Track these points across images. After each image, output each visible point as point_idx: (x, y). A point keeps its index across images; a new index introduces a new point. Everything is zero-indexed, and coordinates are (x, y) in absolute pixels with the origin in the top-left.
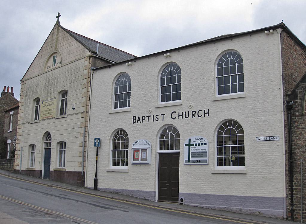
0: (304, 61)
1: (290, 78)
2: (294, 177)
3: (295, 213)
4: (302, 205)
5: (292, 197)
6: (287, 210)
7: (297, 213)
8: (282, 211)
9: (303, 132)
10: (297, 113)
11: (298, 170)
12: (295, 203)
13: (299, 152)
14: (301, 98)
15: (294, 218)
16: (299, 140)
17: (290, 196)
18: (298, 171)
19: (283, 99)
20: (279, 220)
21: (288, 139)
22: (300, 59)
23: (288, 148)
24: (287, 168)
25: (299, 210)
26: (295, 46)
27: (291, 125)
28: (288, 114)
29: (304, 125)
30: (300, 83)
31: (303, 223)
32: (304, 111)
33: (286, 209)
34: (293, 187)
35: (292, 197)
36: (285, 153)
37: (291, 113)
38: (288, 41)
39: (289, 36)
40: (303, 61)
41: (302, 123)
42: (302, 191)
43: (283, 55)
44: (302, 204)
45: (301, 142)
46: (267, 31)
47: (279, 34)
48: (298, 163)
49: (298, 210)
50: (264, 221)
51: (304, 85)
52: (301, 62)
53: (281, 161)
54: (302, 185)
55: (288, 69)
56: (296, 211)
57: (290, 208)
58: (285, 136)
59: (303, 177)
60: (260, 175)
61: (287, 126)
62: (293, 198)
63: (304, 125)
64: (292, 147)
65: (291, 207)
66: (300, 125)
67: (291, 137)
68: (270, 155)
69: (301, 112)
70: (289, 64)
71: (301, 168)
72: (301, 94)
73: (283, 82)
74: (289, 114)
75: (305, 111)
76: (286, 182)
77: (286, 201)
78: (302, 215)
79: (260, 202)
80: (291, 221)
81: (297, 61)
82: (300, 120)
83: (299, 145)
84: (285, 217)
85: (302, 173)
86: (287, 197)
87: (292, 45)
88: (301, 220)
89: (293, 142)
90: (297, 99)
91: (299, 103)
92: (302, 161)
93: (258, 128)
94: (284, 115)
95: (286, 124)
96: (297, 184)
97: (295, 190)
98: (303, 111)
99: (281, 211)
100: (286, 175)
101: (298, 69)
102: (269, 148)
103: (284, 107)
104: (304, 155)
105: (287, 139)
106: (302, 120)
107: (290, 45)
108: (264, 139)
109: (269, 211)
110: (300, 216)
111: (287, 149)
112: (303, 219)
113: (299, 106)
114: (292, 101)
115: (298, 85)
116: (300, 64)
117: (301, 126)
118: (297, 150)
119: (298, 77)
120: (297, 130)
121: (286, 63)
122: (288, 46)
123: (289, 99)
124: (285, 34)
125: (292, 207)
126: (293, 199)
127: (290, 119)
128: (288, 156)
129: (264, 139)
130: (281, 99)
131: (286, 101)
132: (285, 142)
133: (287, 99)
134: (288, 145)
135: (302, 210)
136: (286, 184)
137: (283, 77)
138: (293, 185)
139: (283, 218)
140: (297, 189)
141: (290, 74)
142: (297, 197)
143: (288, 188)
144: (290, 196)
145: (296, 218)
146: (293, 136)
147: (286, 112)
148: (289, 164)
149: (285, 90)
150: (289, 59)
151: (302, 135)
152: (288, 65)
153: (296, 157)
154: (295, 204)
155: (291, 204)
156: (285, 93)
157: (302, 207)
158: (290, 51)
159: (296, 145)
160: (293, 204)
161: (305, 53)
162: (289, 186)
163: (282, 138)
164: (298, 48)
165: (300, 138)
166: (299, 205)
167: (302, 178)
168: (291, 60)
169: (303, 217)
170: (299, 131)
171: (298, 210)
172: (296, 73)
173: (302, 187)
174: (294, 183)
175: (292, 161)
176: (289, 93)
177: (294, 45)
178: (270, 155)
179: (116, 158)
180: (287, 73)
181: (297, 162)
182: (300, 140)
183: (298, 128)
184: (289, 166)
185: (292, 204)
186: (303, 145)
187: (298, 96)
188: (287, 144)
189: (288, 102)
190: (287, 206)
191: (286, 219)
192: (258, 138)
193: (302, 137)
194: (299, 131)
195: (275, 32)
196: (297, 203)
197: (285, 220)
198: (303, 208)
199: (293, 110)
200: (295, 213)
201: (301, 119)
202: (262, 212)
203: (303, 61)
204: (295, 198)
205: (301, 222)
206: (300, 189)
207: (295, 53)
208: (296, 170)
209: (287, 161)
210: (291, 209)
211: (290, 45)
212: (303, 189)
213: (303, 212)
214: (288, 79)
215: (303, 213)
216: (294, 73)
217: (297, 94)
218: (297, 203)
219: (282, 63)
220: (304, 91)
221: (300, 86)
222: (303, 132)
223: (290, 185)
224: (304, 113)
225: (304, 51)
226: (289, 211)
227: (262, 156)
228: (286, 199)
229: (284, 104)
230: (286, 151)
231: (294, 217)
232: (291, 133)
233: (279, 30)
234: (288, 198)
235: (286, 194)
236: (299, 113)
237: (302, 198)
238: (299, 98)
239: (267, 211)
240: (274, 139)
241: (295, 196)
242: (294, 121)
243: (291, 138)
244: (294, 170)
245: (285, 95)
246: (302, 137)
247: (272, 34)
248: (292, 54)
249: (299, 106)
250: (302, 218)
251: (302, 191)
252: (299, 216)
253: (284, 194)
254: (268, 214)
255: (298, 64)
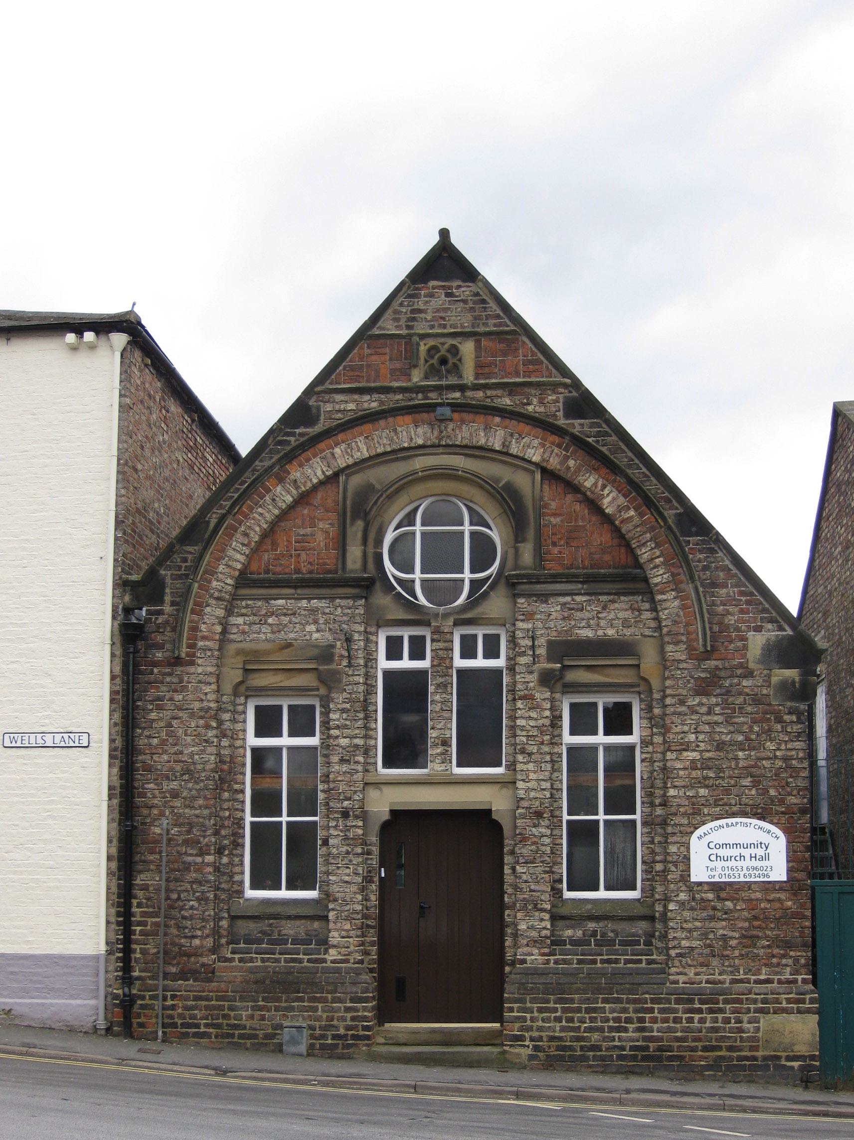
0: (189, 455)
1: (141, 522)
2: (138, 882)
3: (134, 1010)
4: (161, 978)
5: (127, 951)
6: (109, 999)
7: (142, 1007)
8: (93, 1002)
9: (175, 723)
10: (159, 655)
11: (151, 857)
12: (136, 974)
13: (157, 792)
14: (178, 599)
15: (135, 1025)
16: (160, 751)
17: (120, 950)
18: (152, 862)
19: (113, 597)
20: (81, 1035)
21: (120, 746)
22: (179, 449)
23: (121, 778)
24: (114, 851)
25: (152, 998)
26: (165, 402)
27: (133, 695)
28: (125, 654)
29: (181, 697)
30: (177, 547)
31: (163, 1041)
32: (184, 646)
33: (106, 997)
34: (133, 919)
35: (127, 951)
36: (109, 795)
37: (136, 652)
38: (143, 383)
39: (149, 362)
40: (185, 457)
41: (175, 691)
42: (161, 933)
43: (126, 432)
44: (161, 975)
45: (165, 757)
46: (73, 335)
47: (118, 355)
48: (154, 833)
49: (148, 997)
50: (26, 1041)
51: (190, 553)
52: (178, 461)
53: (92, 822)
54: (163, 910)
55: (136, 485)
56: (139, 1002)
57: (120, 992)
58: (110, 734)
59: (167, 880)
60: (15, 873)
61: (119, 697)
62: (133, 956)
63: (181, 697)
64: (132, 775)
65: (123, 988)
66: (168, 696)
67: (133, 737)
68: (51, 802)
69: (174, 653)
70: (139, 467)
71: (164, 849)
72: (178, 584)
73: (115, 535)
74: (131, 656)
75: (188, 647)
76: (108, 900)
77: (106, 967)
78: (160, 1015)
79: (12, 973)
80: (121, 1038)
81: (166, 456)
82: (168, 679)
83: (159, 767)
84: (102, 1024)
85: (164, 866)
86: (109, 953)
87: (154, 398)
88: (156, 1032)
89: (140, 758)
90: (161, 602)
91: (170, 615)
92: (168, 824)
93: (13, 698)
94: (113, 655)
95: (118, 688)
96: (147, 907)
97: (139, 928)
98: (179, 648)
99: (86, 1002)
100: (110, 873)
101: (168, 488)
102: (51, 775)
103: (112, 626)
104: (176, 804)
105: (119, 743)
106: (175, 680)
107: (150, 396)
108: (32, 740)
109: (43, 1005)
110: (154, 1020)
111: (117, 783)
112: (163, 1027)
113: (168, 629)
114: (144, 609)
115: (169, 551)
116: (175, 466)
117: (171, 699)
118: (151, 786)
119: (165, 518)
120: (153, 715)
121: (130, 464)
122: (142, 402)
123: (132, 600)
124: (138, 354)
125: (126, 989)
126: (130, 961)
127: (134, 674)
128: (120, 806)
129: (32, 740)
130: (104, 595)
131: (121, 607)
132: (111, 757)
133: (127, 598)
134: (121, 767)
135: (161, 996)
136: (107, 908)
137: (117, 517)
138: (134, 909)
139: (95, 1029)
140: (144, 924)
141: (140, 505)
142: (144, 952)
143: (113, 919)
144: (120, 950)
145: (141, 1025)
146: (141, 735)
147: (118, 644)
148: (121, 834)
149: (123, 564)
150: (142, 448)
151: (172, 731)
152: (136, 470)
153: (145, 811)
154: (138, 978)
155: (123, 978)
156: (120, 578)
157: (161, 988)
158: (148, 420)
159: (148, 769)
160: (131, 977)
161: (194, 427)
162: (118, 914)
163: (101, 741)
164: (175, 408)
165: (163, 742)
166: (151, 982)
167: (163, 883)
168: (147, 452)
169: (163, 1024)
170: (161, 719)
171: (148, 997)
172: (159, 500)
173: (165, 917)
174: (135, 902)
175: (132, 826)
176: (135, 577)
177: (162, 399)
178: (51, 802)
179: (285, 819)
180: (132, 501)
181: (150, 829)
182: (165, 752)
183: (160, 708)
184: (120, 841)
185: (127, 979)
186: (171, 769)
187: (168, 590)
188: (117, 762)
189: (128, 611)
190: (110, 986)
191: (103, 1032)
192: (12, 735)
193: (171, 740)
194: (161, 719)
195: (103, 340)
196: (143, 974)
197: (101, 1035)
198: (163, 991)
199: (146, 639)
200: (136, 1009)
201: (170, 674)
202: (18, 1010)
203: (185, 457)
204: (138, 955)
205: (156, 1039)
206: (157, 924)
207: (163, 425)
208: (143, 858)
209: (115, 825)
210: (125, 995)
211: (150, 396)
212: (166, 926)
213: (163, 1005)
214: (134, 523)
215: (165, 1008)
216: (154, 502)
217: (162, 586)
218: (143, 974)
219: (118, 464)
220: (187, 576)
221: (175, 556)
222: (175, 723)
223: (122, 910)
224: (183, 655)
225: (193, 421)
226: (118, 1002)
227: (23, 803)
228: (107, 961)
229: (114, 618)
230: (110, 788)
231: (135, 1021)
232: (132, 724)
233: (120, 339)
234: (113, 958)
235: (107, 943)
236: (168, 654)
237: (161, 955)
238: (168, 598)
239: (38, 1004)
240: (72, 744)
241: (138, 950)
242: (146, 679)
243: (133, 741)
244: (137, 858)
245: (122, 584)
246: (171, 740)
247: (92, 347)
248: (154, 428)
249: (168, 629)
250: (160, 1025)
251: (161, 933)
252: (151, 1017)
253: (98, 944)
254: (39, 1016)
255: (170, 467)
